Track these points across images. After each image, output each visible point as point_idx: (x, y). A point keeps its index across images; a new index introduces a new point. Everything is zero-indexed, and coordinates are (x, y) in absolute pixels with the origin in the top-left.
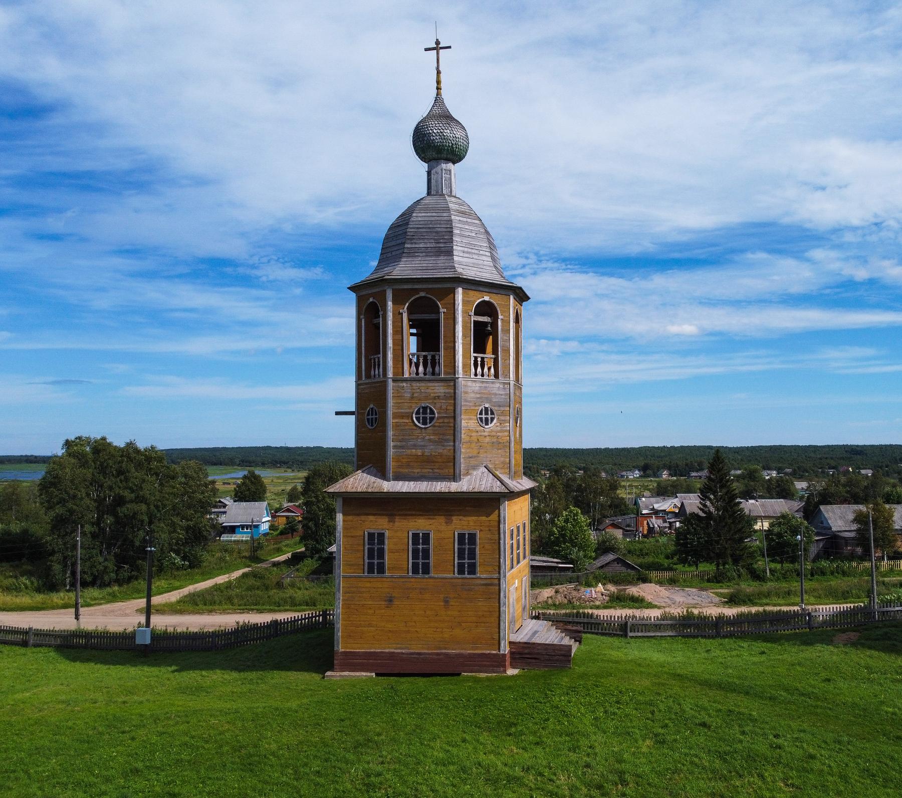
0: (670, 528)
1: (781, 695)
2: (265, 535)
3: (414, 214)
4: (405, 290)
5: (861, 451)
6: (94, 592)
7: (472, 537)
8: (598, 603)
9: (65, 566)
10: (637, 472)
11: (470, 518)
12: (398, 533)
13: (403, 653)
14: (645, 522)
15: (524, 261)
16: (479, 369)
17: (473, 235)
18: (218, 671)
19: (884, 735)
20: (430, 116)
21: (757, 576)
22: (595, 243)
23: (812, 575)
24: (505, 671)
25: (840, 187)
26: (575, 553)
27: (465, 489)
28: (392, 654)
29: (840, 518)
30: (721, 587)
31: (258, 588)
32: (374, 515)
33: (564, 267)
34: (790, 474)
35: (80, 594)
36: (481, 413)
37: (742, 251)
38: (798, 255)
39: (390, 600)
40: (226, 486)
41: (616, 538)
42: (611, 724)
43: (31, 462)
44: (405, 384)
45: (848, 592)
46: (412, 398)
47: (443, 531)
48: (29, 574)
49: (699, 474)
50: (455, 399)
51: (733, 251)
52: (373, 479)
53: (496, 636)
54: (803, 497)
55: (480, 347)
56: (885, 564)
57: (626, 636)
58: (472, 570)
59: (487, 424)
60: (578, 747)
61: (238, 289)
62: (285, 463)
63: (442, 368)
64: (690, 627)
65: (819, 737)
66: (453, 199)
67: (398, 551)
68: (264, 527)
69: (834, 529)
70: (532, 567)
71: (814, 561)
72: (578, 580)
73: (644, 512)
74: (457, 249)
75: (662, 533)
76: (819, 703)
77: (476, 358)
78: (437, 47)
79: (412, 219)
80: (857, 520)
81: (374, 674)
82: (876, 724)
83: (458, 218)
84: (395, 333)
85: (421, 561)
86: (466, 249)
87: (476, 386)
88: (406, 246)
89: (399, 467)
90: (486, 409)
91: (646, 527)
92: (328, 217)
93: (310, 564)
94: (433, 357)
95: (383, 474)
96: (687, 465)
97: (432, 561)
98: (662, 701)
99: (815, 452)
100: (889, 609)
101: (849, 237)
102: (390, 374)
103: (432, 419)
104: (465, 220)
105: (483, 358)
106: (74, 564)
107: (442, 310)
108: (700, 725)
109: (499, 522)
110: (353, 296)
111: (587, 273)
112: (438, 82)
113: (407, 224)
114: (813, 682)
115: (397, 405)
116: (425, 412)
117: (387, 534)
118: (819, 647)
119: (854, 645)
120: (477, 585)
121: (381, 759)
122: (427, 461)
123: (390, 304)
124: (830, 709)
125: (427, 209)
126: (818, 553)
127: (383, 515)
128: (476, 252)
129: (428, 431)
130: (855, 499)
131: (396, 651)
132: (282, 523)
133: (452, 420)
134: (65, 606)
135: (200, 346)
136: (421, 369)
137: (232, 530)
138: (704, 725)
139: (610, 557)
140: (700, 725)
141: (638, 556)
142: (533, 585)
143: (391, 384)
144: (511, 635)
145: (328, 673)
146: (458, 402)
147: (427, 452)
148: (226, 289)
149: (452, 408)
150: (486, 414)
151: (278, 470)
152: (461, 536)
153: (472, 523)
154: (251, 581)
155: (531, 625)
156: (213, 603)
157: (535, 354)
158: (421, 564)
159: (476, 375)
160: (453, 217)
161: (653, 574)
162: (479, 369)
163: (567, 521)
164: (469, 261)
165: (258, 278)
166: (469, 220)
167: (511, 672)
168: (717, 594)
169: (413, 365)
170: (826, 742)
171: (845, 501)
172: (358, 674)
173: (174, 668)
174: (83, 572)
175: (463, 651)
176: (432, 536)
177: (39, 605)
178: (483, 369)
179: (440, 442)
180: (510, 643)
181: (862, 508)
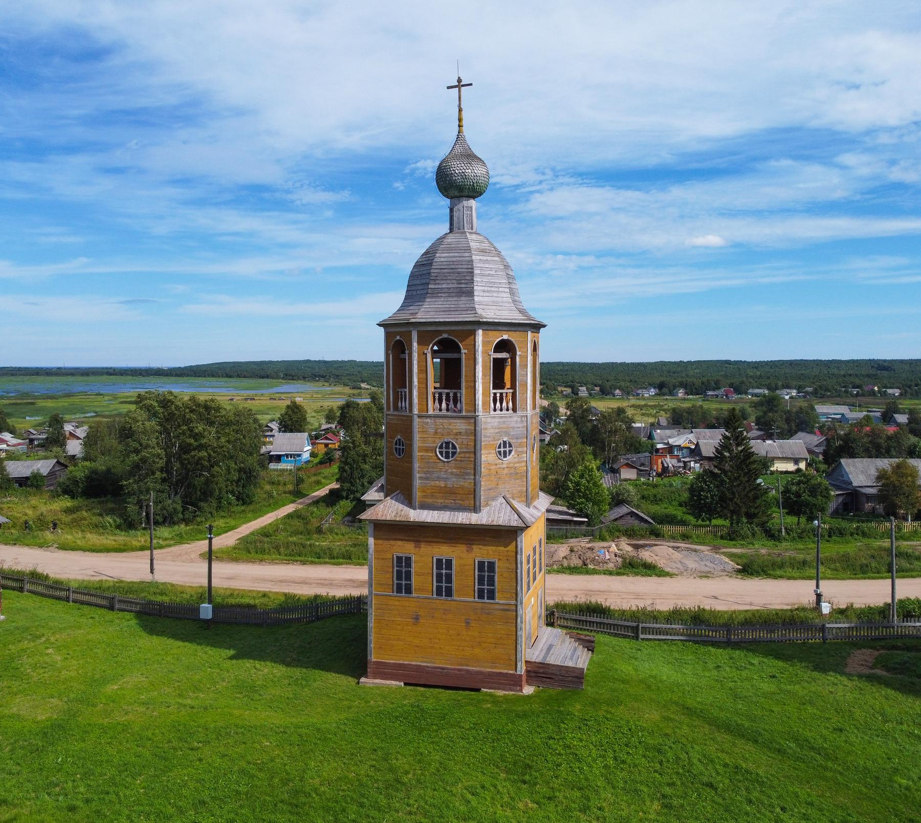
0: (684, 468)
1: (790, 748)
2: (307, 462)
3: (437, 255)
4: (428, 332)
5: (889, 367)
6: (164, 532)
7: (491, 565)
8: (611, 566)
9: (141, 507)
10: (652, 390)
11: (489, 548)
12: (424, 558)
13: (428, 667)
14: (660, 461)
15: (540, 177)
16: (498, 404)
17: (493, 273)
18: (268, 663)
20: (452, 156)
21: (771, 535)
22: (611, 156)
23: (830, 536)
24: (521, 691)
25: (876, 85)
26: (589, 507)
27: (484, 522)
28: (418, 668)
29: (862, 472)
30: (735, 546)
32: (402, 540)
33: (581, 182)
34: (811, 393)
35: (154, 532)
36: (500, 447)
37: (765, 159)
38: (826, 161)
39: (417, 618)
41: (628, 491)
42: (621, 775)
43: (111, 374)
44: (429, 420)
45: (867, 566)
46: (436, 433)
47: (466, 559)
48: (111, 512)
49: (715, 393)
51: (755, 159)
52: (401, 506)
55: (498, 382)
57: (637, 638)
58: (491, 595)
59: (505, 456)
60: (589, 808)
61: (276, 213)
62: (323, 377)
64: (704, 630)
66: (474, 237)
67: (423, 574)
68: (306, 456)
69: (855, 484)
70: (548, 520)
73: (659, 446)
74: (477, 289)
75: (676, 473)
76: (830, 764)
77: (495, 394)
78: (460, 85)
79: (436, 260)
80: (879, 478)
81: (402, 684)
83: (478, 257)
84: (420, 371)
85: (444, 585)
86: (486, 288)
87: (495, 422)
88: (430, 286)
90: (505, 442)
91: (660, 466)
92: (355, 142)
93: (345, 505)
94: (455, 394)
95: (409, 501)
96: (703, 383)
97: (454, 585)
98: (671, 748)
101: (884, 139)
102: (416, 411)
103: (454, 454)
104: (485, 258)
105: (501, 394)
106: (148, 506)
107: (463, 351)
108: (707, 785)
110: (382, 329)
111: (604, 187)
112: (460, 120)
113: (431, 264)
115: (423, 440)
116: (447, 453)
117: (413, 559)
121: (408, 809)
122: (450, 492)
123: (415, 344)
125: (449, 250)
126: (837, 508)
127: (408, 540)
128: (496, 289)
129: (450, 465)
132: (321, 450)
133: (472, 455)
134: (142, 549)
135: (246, 267)
136: (444, 405)
137: (278, 458)
138: (711, 785)
139: (624, 510)
140: (707, 785)
141: (652, 502)
142: (550, 538)
143: (416, 421)
144: (528, 650)
145: (363, 680)
146: (478, 438)
148: (266, 214)
149: (473, 444)
150: (505, 447)
151: (317, 384)
152: (481, 564)
153: (491, 552)
154: (297, 523)
155: (549, 635)
156: (263, 551)
157: (552, 269)
158: (444, 588)
159: (495, 410)
160: (474, 257)
161: (666, 529)
162: (498, 404)
163: (582, 476)
164: (491, 303)
165: (292, 202)
166: (489, 258)
167: (528, 690)
168: (731, 556)
169: (437, 401)
172: (388, 682)
173: (232, 652)
174: (155, 514)
175: (483, 669)
176: (454, 562)
178: (501, 403)
179: (462, 475)
180: (526, 662)
181: (885, 463)
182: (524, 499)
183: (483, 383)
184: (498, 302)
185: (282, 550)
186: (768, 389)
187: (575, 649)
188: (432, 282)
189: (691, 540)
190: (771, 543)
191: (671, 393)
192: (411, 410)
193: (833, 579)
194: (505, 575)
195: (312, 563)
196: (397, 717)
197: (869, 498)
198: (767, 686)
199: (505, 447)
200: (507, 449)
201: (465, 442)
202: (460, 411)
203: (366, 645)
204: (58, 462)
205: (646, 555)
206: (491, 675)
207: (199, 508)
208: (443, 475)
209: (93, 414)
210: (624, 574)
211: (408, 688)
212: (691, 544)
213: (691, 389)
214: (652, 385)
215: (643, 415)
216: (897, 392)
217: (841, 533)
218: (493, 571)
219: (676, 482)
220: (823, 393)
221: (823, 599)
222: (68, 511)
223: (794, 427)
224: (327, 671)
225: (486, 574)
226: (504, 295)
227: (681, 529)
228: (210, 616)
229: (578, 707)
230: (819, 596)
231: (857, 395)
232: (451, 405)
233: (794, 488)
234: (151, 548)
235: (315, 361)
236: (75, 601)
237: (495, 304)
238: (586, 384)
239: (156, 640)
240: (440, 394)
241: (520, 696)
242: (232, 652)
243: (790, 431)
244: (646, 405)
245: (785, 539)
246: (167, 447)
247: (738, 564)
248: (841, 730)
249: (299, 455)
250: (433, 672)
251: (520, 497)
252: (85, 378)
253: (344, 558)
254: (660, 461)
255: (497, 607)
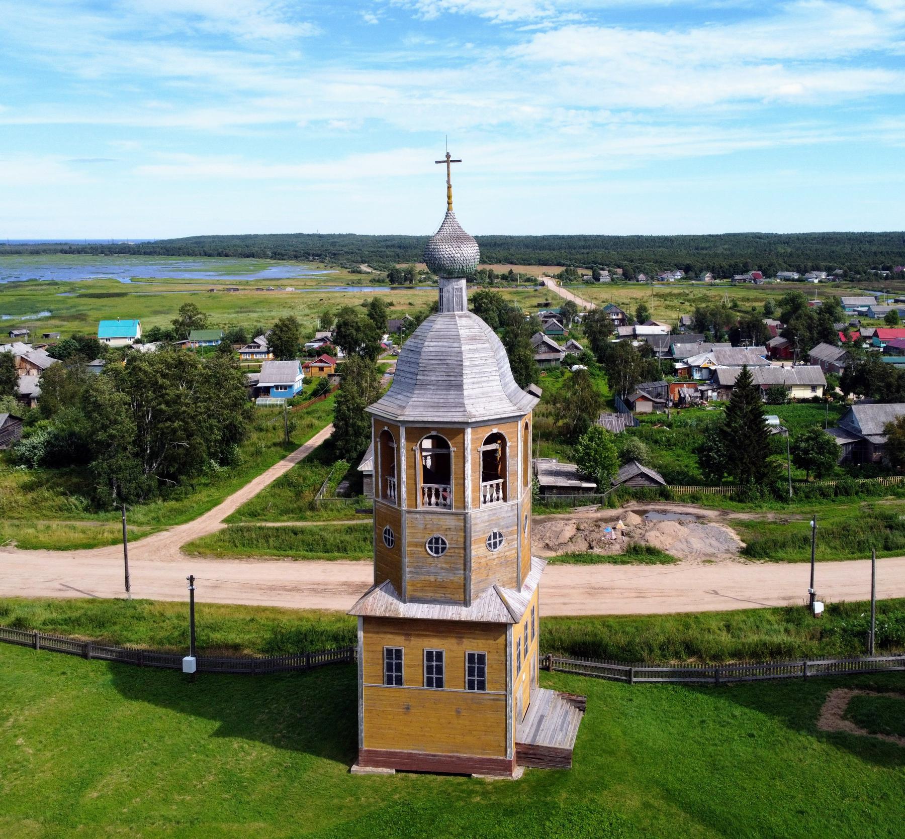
0: (701, 398)
2: (300, 393)
3: (426, 343)
6: (139, 512)
7: (481, 658)
10: (678, 274)
12: (413, 651)
17: (483, 362)
23: (836, 495)
24: (511, 775)
28: (410, 755)
30: (742, 510)
31: (292, 511)
34: (841, 276)
36: (490, 539)
40: (259, 292)
43: (66, 252)
44: (418, 516)
47: (454, 652)
48: (74, 490)
50: (465, 532)
52: (391, 599)
53: (503, 745)
58: (482, 686)
59: (495, 547)
63: (452, 498)
67: (414, 666)
68: (298, 386)
69: (864, 433)
72: (600, 501)
75: (693, 404)
78: (448, 160)
81: (394, 771)
83: (467, 347)
84: (408, 467)
85: (434, 676)
86: (475, 380)
87: (485, 516)
88: (419, 377)
89: (414, 590)
90: (495, 534)
95: (399, 593)
97: (445, 677)
99: (870, 242)
102: (404, 507)
103: (443, 549)
104: (474, 347)
107: (452, 449)
109: (506, 646)
112: (449, 197)
117: (403, 652)
120: (486, 699)
122: (439, 586)
123: (403, 441)
128: (486, 379)
131: (414, 752)
133: (462, 551)
134: (114, 542)
136: (433, 500)
143: (406, 518)
145: (354, 768)
147: (439, 578)
149: (462, 540)
152: (471, 657)
153: (481, 645)
154: (288, 493)
158: (434, 673)
160: (464, 348)
161: (677, 490)
166: (479, 346)
168: (738, 525)
169: (426, 496)
173: (217, 725)
176: (444, 654)
177: (92, 542)
179: (452, 570)
180: (516, 744)
182: (515, 584)
183: (472, 480)
184: (487, 393)
185: (271, 540)
186: (798, 272)
187: (567, 712)
188: (420, 373)
189: (700, 503)
190: (779, 505)
191: (698, 277)
192: (400, 505)
194: (495, 666)
195: (305, 558)
196: (386, 823)
197: (877, 447)
198: (743, 750)
199: (495, 538)
200: (498, 540)
201: (455, 538)
202: (450, 507)
203: (357, 701)
204: (10, 416)
205: (654, 539)
206: (482, 761)
207: (179, 482)
208: (433, 570)
209: (47, 314)
210: (628, 563)
211: (401, 775)
212: (700, 508)
213: (719, 273)
214: (678, 267)
215: (667, 307)
218: (483, 663)
219: (695, 413)
221: (816, 598)
222: (27, 488)
223: (815, 335)
224: (318, 755)
225: (476, 665)
226: (495, 383)
227: (691, 489)
228: (193, 669)
229: (564, 795)
230: (812, 595)
231: (887, 278)
232: (441, 500)
233: (803, 445)
234: (124, 541)
235: (308, 235)
236: (42, 648)
237: (485, 395)
238: (608, 266)
239: (136, 706)
240: (430, 489)
241: (510, 781)
242: (217, 725)
243: (811, 339)
244: (670, 294)
245: (792, 500)
246: (139, 418)
247: (743, 541)
248: (802, 812)
249: (291, 387)
250: (425, 759)
251: (511, 583)
252: (35, 258)
253: (339, 551)
254: (677, 389)
255: (487, 697)
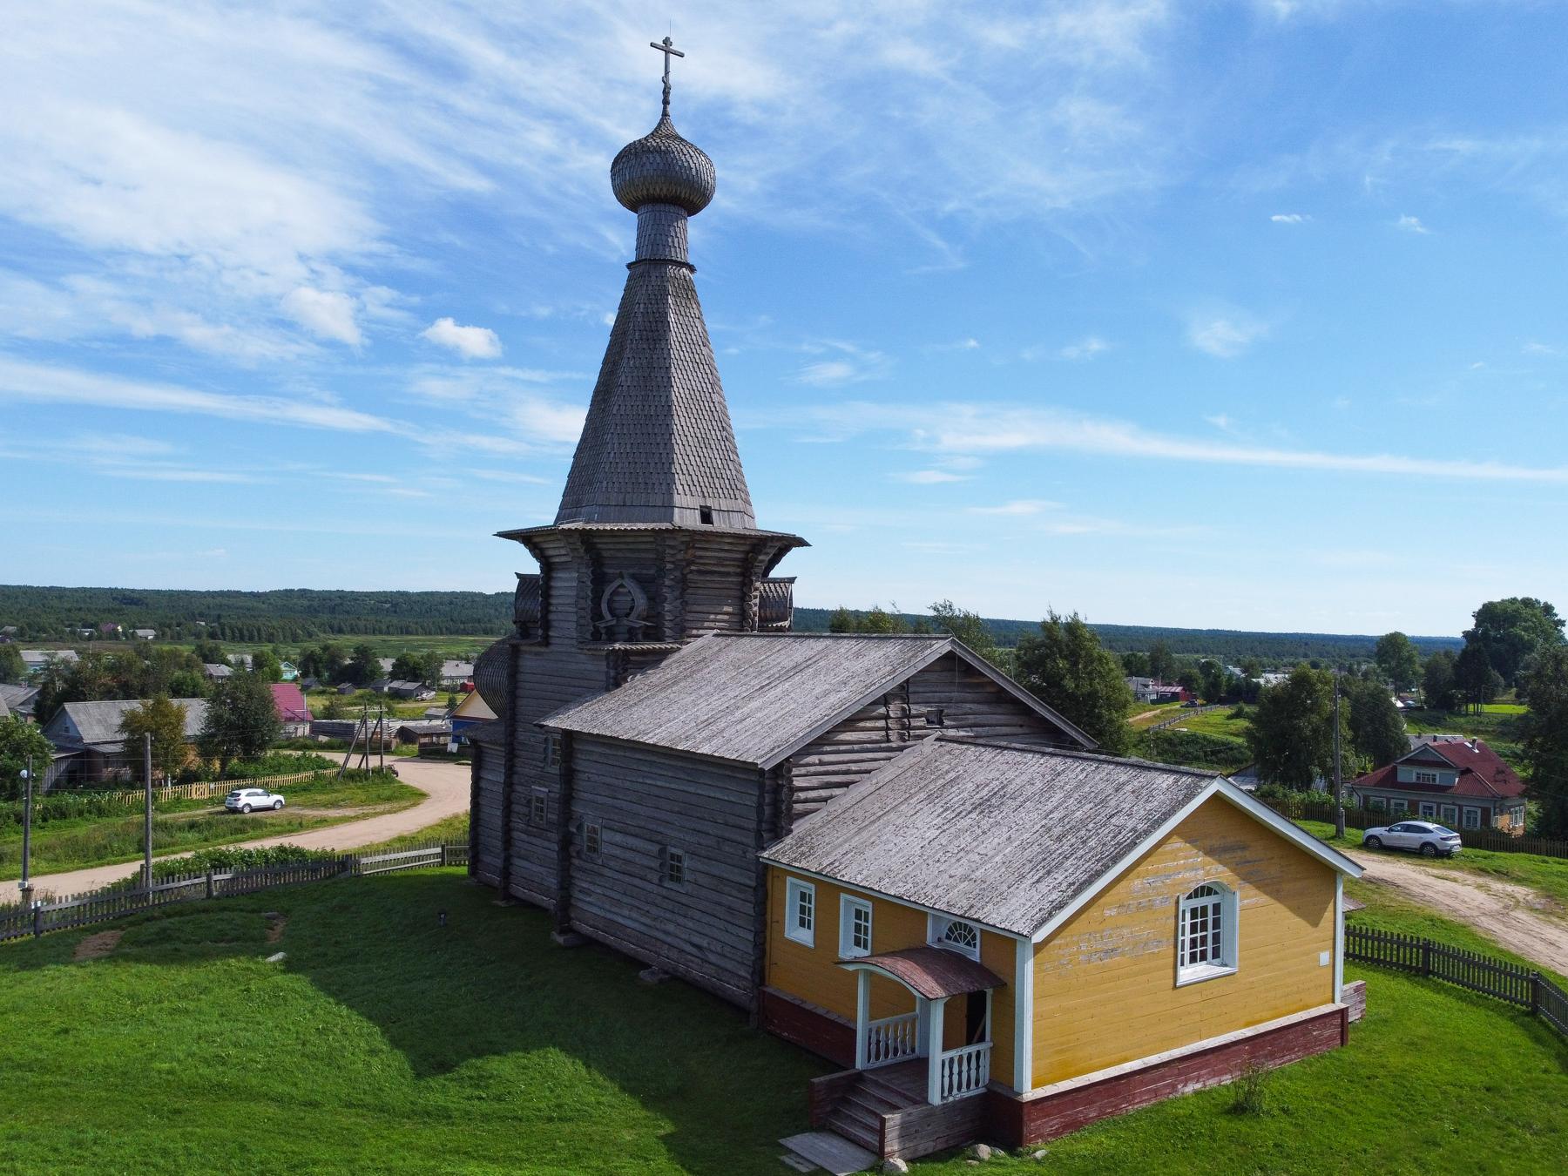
19: (154, 1112)
23: (45, 820)
29: (97, 722)
34: (14, 635)
54: (35, 677)
56: (169, 791)
65: (45, 1142)
71: (49, 794)
76: (48, 1078)
80: (124, 727)
82: (142, 1095)
100: (171, 885)
101: (135, 268)
114: (37, 1040)
118: (51, 971)
119: (115, 956)
124: (66, 1085)
130: (126, 691)
170: (56, 1150)
171: (109, 695)
181: (136, 705)
193: (51, 873)
216: (150, 634)
217: (62, 814)
220: (33, 634)
231: (90, 638)
